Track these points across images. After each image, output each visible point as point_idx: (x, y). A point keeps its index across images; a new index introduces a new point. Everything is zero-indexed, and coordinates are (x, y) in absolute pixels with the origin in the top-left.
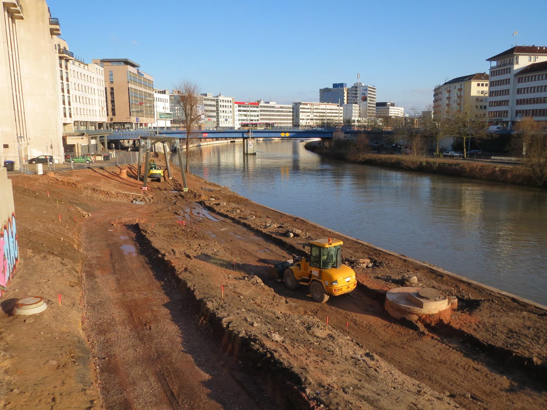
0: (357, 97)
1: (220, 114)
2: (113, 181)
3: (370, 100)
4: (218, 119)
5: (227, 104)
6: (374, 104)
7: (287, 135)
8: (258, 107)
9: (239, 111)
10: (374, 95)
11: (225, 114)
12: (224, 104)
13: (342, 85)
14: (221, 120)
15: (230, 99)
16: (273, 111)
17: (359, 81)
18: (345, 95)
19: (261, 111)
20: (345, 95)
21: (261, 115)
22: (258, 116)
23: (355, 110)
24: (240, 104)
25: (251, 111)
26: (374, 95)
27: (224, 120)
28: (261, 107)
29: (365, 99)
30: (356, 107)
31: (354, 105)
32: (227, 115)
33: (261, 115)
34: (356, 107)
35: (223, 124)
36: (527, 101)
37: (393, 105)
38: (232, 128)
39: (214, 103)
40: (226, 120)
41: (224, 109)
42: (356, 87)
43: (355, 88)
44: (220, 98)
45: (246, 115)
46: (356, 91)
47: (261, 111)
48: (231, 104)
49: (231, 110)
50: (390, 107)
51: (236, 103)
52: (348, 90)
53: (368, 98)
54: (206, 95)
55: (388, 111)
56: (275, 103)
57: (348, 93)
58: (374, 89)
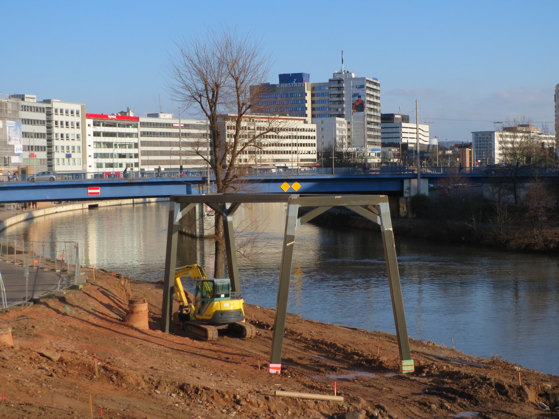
0: (341, 102)
1: (56, 143)
2: (168, 346)
3: (371, 109)
4: (50, 153)
5: (70, 119)
6: (377, 117)
7: (297, 186)
8: (136, 126)
9: (96, 134)
10: (377, 98)
11: (65, 143)
12: (64, 118)
13: (299, 77)
14: (58, 155)
15: (77, 107)
16: (169, 135)
17: (344, 68)
18: (308, 98)
19: (144, 134)
20: (308, 98)
21: (144, 144)
22: (136, 146)
23: (341, 130)
24: (99, 119)
25: (121, 135)
26: (377, 98)
27: (63, 155)
28: (143, 124)
29: (359, 107)
30: (341, 123)
31: (338, 119)
32: (70, 143)
33: (144, 144)
34: (341, 123)
35: (62, 166)
36: (38, 123)
37: (406, 119)
38: (77, 175)
39: (42, 116)
40: (69, 156)
41: (64, 131)
42: (339, 81)
43: (337, 82)
44: (56, 105)
45: (109, 145)
46: (340, 88)
47: (144, 134)
48: (78, 119)
49: (79, 131)
50: (404, 125)
51: (89, 116)
52: (313, 89)
53: (368, 105)
54: (23, 98)
55: (399, 133)
56: (169, 116)
57: (313, 95)
58: (375, 84)
